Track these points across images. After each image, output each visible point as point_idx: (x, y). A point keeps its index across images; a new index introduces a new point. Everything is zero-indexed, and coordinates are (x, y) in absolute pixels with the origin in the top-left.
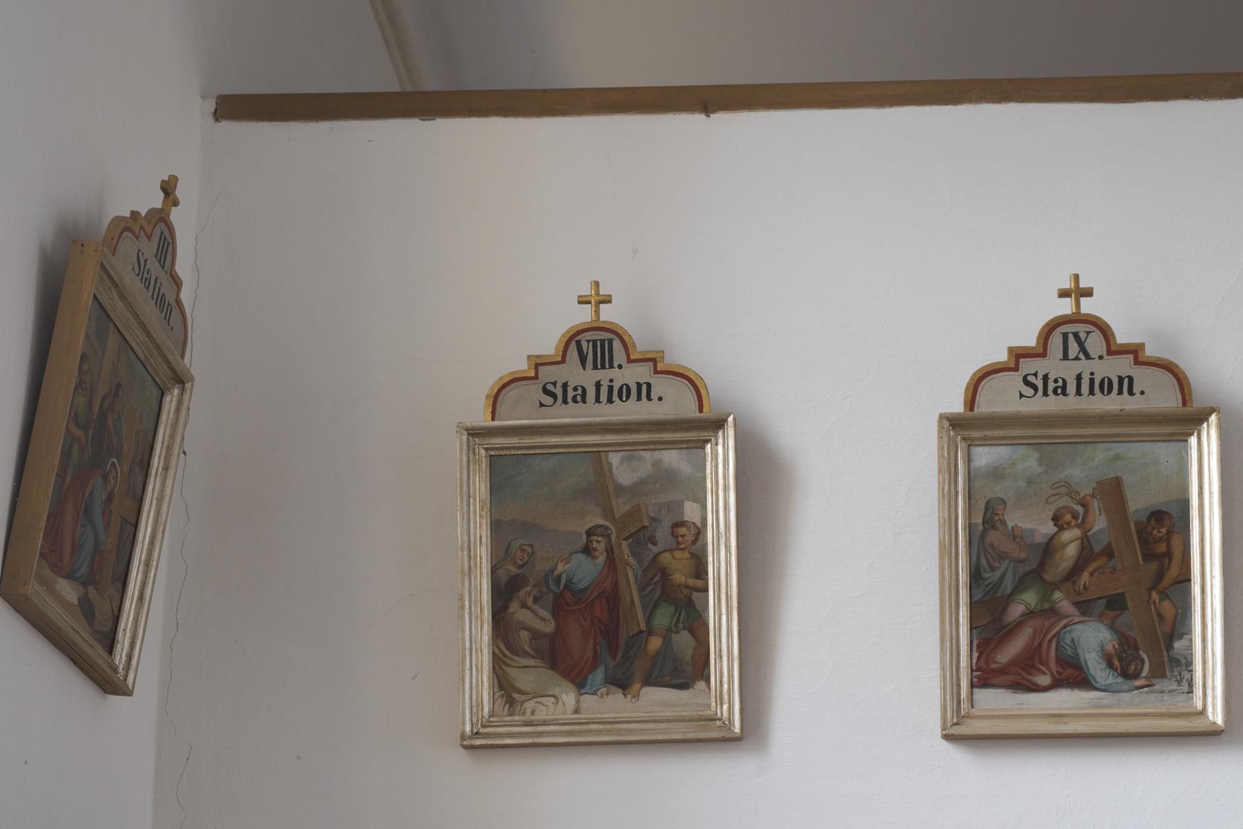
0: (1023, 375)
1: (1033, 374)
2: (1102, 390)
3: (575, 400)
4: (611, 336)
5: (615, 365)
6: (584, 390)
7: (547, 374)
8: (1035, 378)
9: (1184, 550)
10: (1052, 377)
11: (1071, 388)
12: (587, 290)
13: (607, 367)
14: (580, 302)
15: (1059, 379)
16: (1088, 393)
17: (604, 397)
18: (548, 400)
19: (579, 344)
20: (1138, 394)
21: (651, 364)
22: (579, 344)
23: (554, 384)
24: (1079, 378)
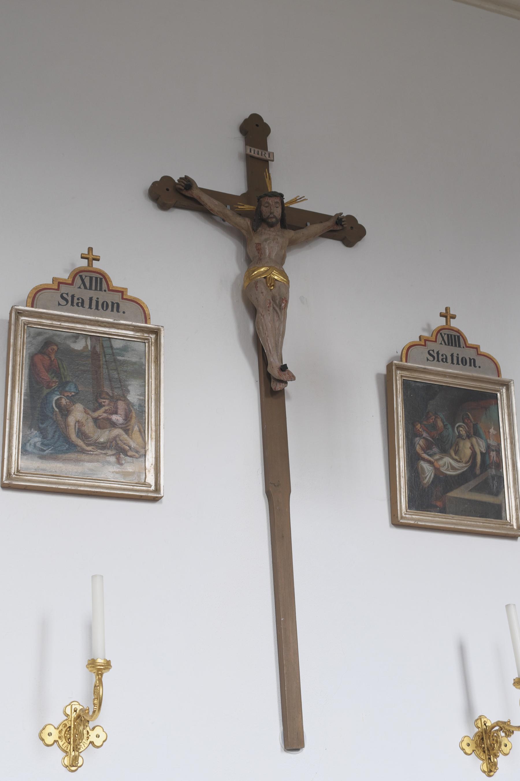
0: (61, 293)
1: (66, 294)
2: (462, 363)
3: (77, 304)
4: (101, 277)
5: (103, 290)
6: (83, 300)
7: (64, 289)
8: (67, 296)
9: (11, 421)
10: (441, 353)
11: (449, 360)
13: (98, 289)
14: (82, 258)
15: (444, 355)
16: (95, 308)
17: (455, 361)
18: (63, 302)
19: (441, 334)
20: (478, 367)
21: (120, 294)
22: (441, 334)
23: (67, 294)
24: (91, 299)
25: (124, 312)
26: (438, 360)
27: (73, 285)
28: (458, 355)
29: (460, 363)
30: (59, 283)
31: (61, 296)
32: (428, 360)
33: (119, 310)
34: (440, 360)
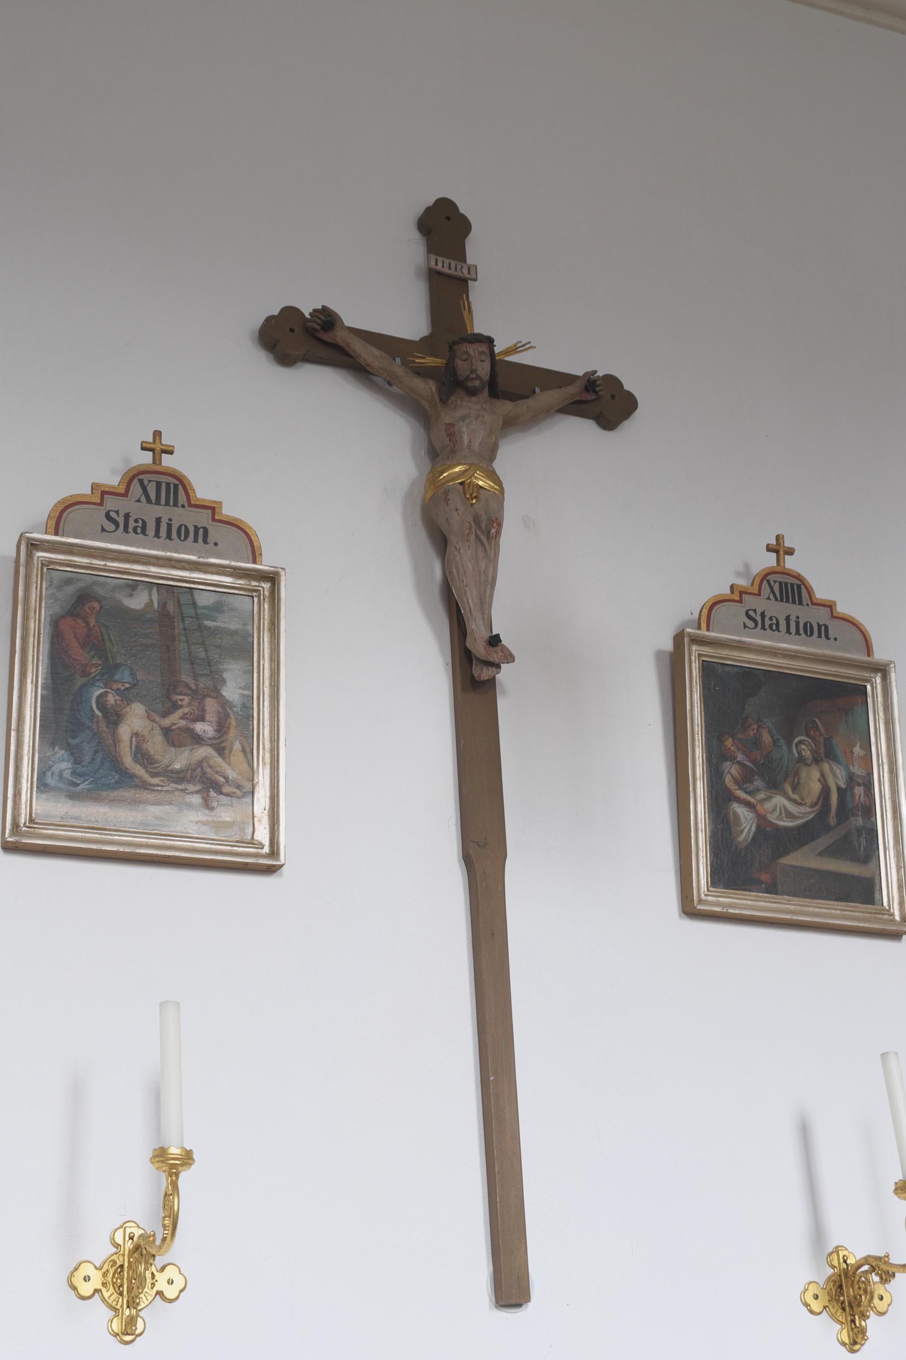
0: (107, 510)
1: (115, 511)
2: (806, 632)
3: (135, 530)
4: (177, 482)
5: (180, 505)
6: (144, 523)
7: (111, 503)
8: (116, 515)
10: (768, 615)
11: (783, 627)
12: (166, 440)
13: (172, 504)
14: (143, 449)
15: (773, 618)
16: (165, 537)
17: (793, 629)
18: (110, 526)
19: (768, 581)
20: (832, 640)
21: (210, 512)
22: (768, 581)
23: (117, 512)
24: (158, 521)
25: (216, 544)
26: (763, 628)
27: (127, 497)
28: (798, 617)
29: (802, 631)
30: (103, 493)
31: (106, 516)
32: (745, 626)
33: (207, 540)
34: (767, 626)
